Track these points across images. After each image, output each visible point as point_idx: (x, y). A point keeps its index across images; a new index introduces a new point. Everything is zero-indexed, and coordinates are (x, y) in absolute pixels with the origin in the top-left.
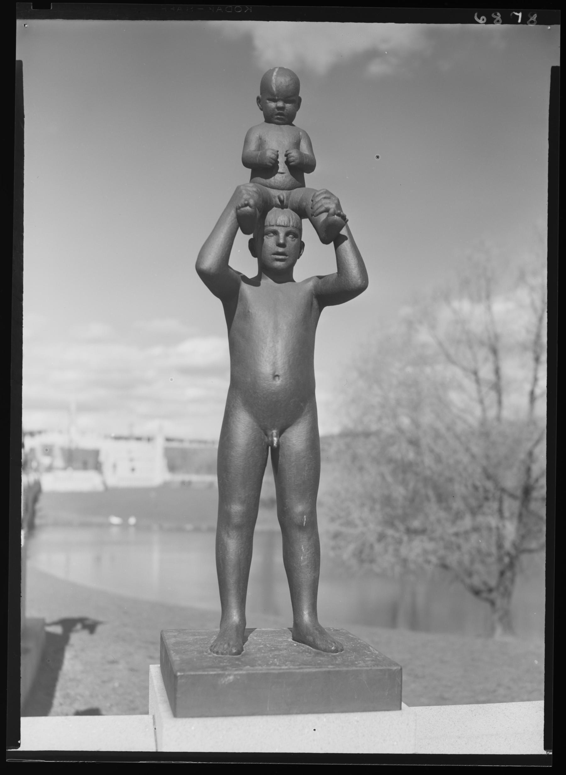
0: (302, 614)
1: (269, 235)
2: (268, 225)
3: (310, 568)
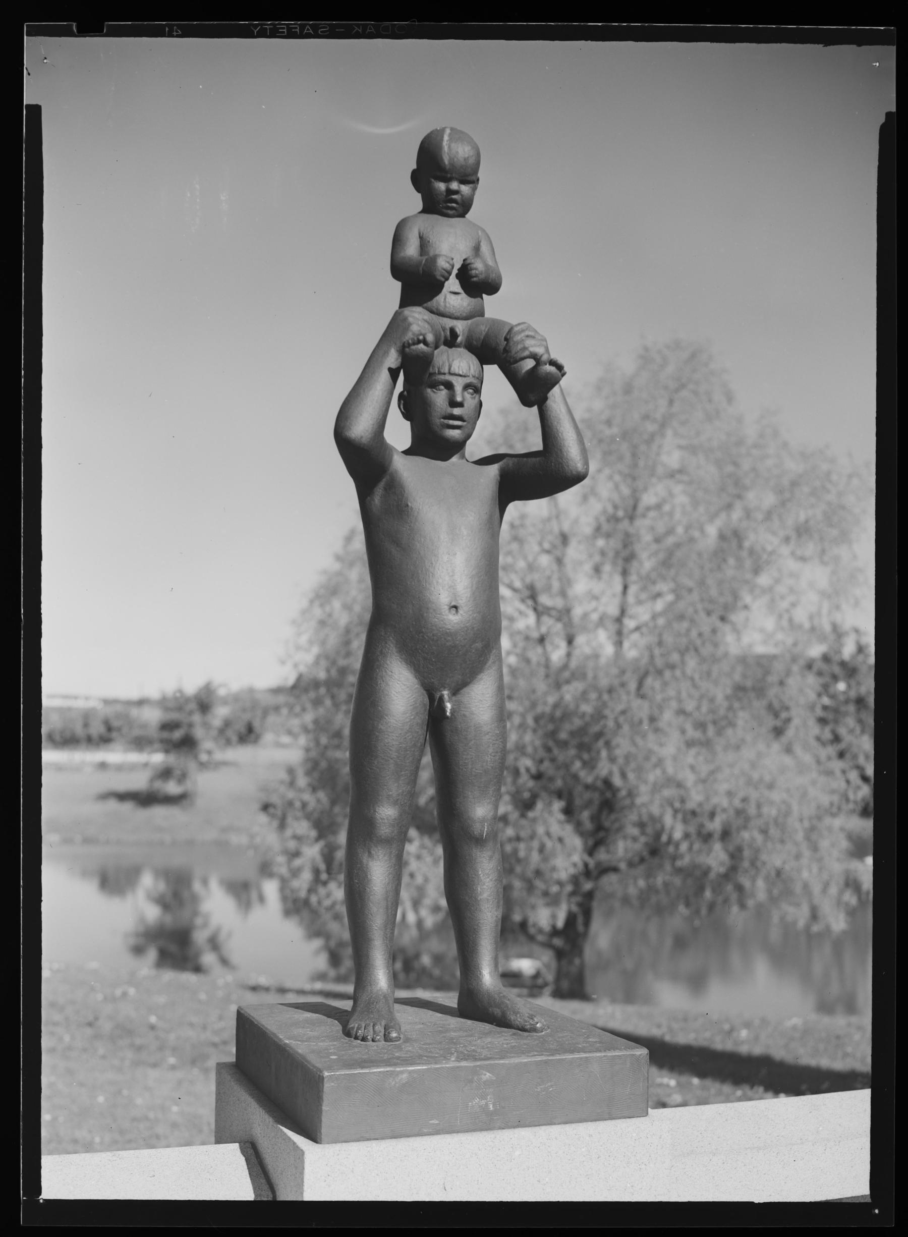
0: (480, 974)
1: (437, 387)
2: (437, 372)
3: (491, 903)
